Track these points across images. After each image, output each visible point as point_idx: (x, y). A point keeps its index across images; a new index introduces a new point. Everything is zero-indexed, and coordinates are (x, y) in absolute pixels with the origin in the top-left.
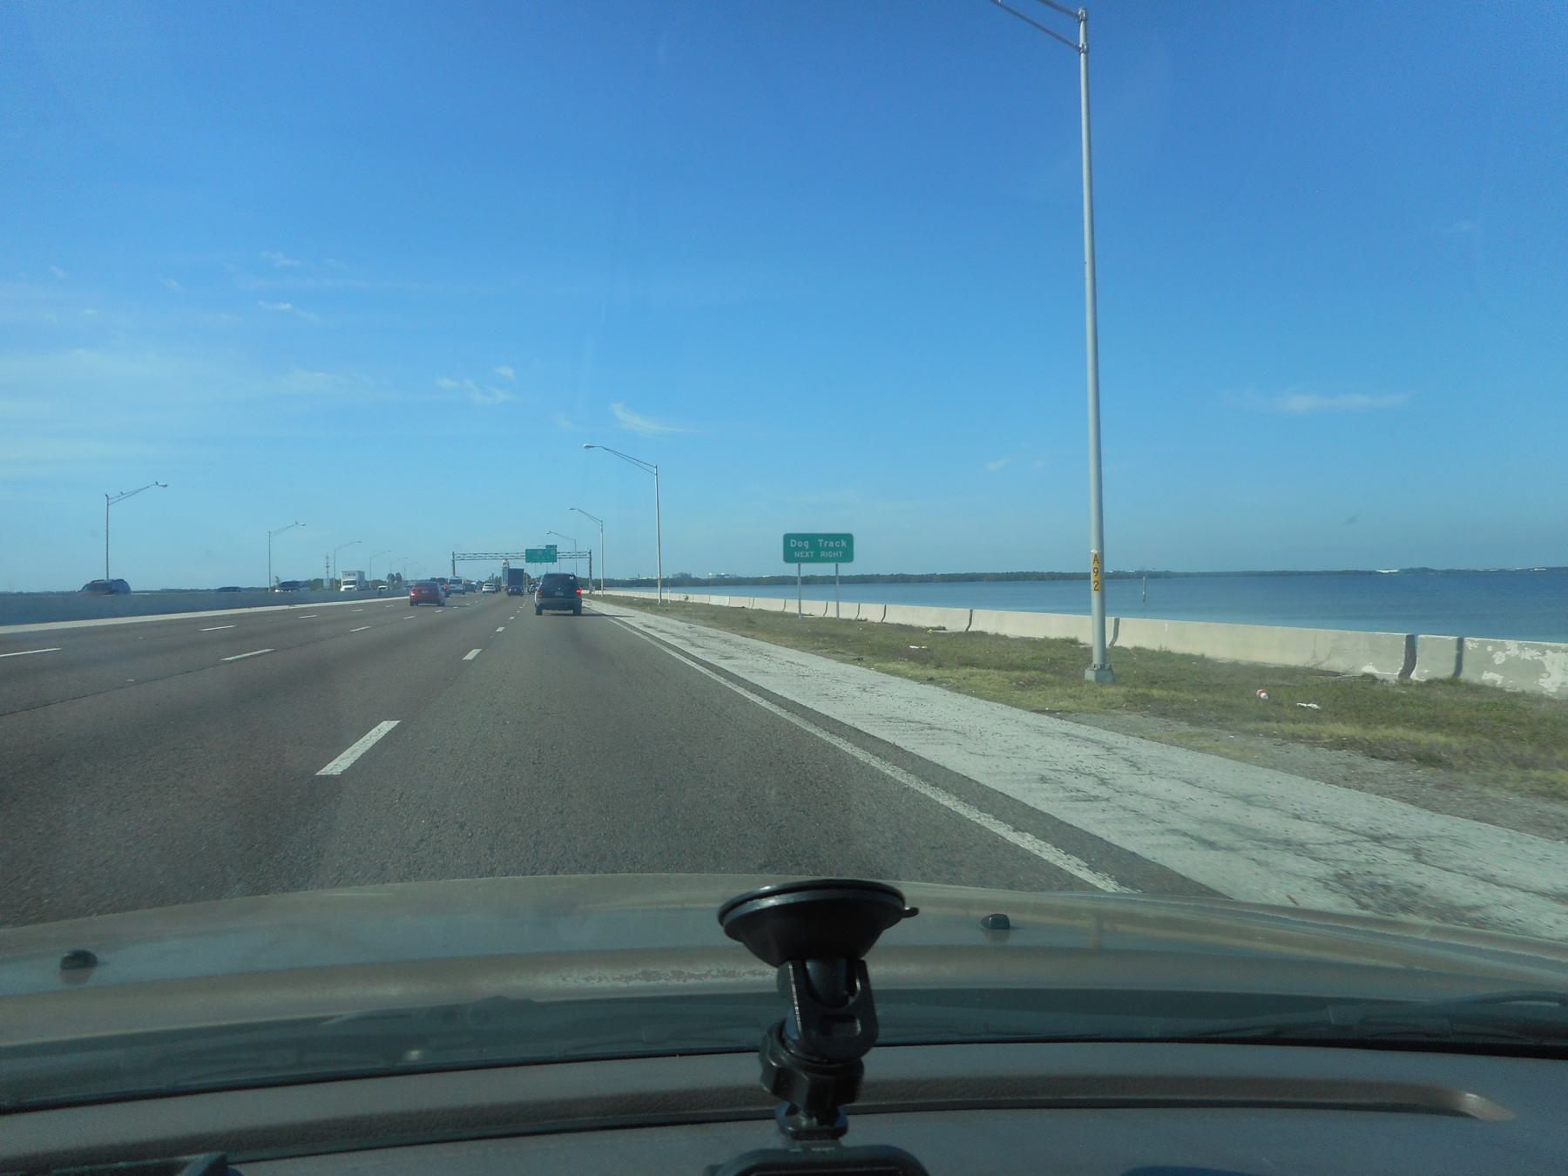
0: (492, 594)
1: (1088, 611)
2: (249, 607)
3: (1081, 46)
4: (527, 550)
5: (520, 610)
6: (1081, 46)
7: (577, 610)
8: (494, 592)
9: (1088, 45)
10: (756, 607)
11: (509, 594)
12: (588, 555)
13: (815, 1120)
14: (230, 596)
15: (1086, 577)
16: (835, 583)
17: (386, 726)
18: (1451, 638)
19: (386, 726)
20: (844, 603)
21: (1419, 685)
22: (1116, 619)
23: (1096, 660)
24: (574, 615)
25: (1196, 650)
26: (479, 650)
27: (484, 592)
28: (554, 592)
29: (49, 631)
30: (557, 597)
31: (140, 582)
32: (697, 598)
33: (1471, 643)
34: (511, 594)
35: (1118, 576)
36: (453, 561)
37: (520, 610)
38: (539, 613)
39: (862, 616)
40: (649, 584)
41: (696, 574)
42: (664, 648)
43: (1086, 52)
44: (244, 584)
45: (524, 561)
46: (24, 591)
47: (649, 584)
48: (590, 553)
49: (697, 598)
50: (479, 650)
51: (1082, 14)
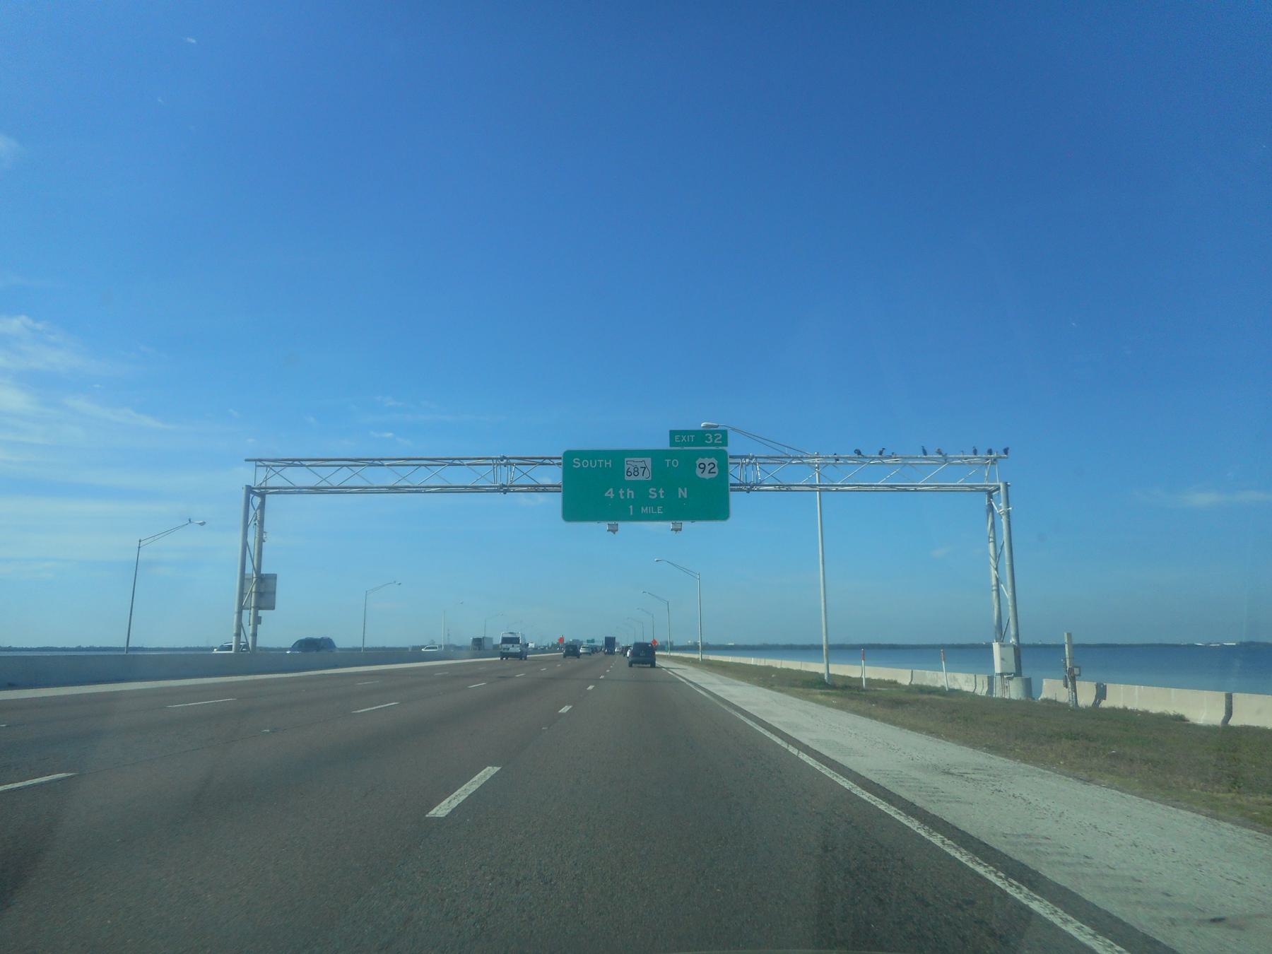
0: (588, 656)
1: (823, 662)
2: (419, 661)
5: (605, 674)
7: (653, 665)
8: (590, 654)
10: (784, 667)
11: (606, 654)
14: (64, 649)
16: (1076, 648)
17: (490, 771)
18: (1044, 684)
19: (490, 771)
20: (1082, 683)
21: (1232, 728)
22: (1227, 695)
24: (651, 667)
26: (497, 769)
29: (204, 685)
31: (345, 639)
32: (712, 657)
33: (914, 671)
34: (608, 653)
37: (605, 674)
38: (631, 665)
39: (916, 682)
40: (810, 650)
42: (678, 677)
45: (555, 501)
46: (387, 646)
47: (810, 650)
49: (712, 657)
50: (497, 769)
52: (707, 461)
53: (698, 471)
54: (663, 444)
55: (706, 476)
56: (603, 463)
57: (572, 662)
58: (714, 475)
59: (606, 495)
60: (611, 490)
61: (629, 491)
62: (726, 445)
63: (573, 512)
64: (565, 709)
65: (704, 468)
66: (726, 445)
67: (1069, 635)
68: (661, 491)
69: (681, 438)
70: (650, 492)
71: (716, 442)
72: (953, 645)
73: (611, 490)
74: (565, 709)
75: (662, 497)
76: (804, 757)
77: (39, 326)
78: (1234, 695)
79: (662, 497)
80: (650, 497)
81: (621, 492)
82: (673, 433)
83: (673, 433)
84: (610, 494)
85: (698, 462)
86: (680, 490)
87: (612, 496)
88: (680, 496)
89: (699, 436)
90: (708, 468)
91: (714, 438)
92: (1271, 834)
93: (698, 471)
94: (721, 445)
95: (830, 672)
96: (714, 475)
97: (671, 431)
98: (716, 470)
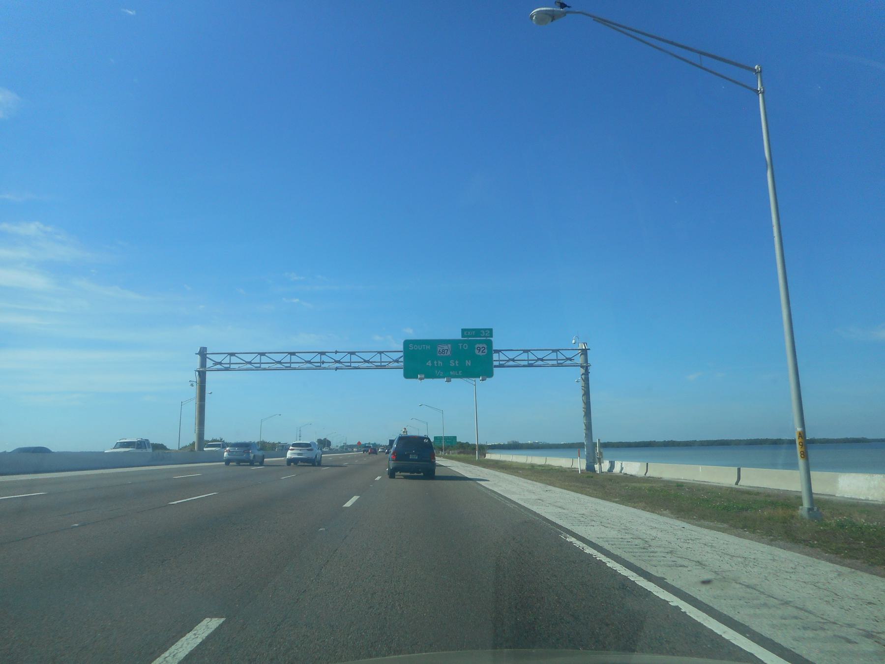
1: (793, 466)
3: (759, 89)
4: (407, 343)
6: (759, 89)
9: (763, 88)
12: (579, 360)
13: (134, 11)
15: (793, 442)
22: (738, 469)
23: (806, 504)
25: (765, 486)
26: (358, 497)
27: (290, 461)
28: (408, 455)
30: (412, 460)
35: (813, 441)
36: (202, 375)
41: (522, 441)
43: (763, 93)
44: (56, 446)
48: (584, 352)
50: (358, 497)
51: (758, 68)
52: (481, 346)
53: (477, 351)
54: (458, 336)
55: (481, 354)
56: (425, 347)
57: (373, 457)
58: (485, 354)
59: (427, 364)
60: (430, 361)
61: (439, 362)
62: (492, 337)
63: (407, 376)
64: (378, 478)
65: (480, 350)
66: (492, 337)
67: (599, 440)
68: (457, 362)
69: (467, 333)
70: (451, 362)
71: (486, 335)
72: (847, 438)
73: (430, 361)
74: (378, 478)
75: (457, 365)
76: (611, 564)
77: (49, 229)
78: (741, 468)
79: (457, 365)
80: (451, 365)
81: (435, 362)
82: (463, 330)
83: (463, 330)
84: (429, 363)
85: (476, 346)
86: (467, 361)
87: (430, 364)
88: (467, 365)
89: (478, 332)
90: (481, 350)
91: (485, 333)
92: (883, 579)
93: (477, 351)
94: (488, 337)
95: (816, 489)
96: (485, 354)
97: (462, 329)
98: (486, 351)
